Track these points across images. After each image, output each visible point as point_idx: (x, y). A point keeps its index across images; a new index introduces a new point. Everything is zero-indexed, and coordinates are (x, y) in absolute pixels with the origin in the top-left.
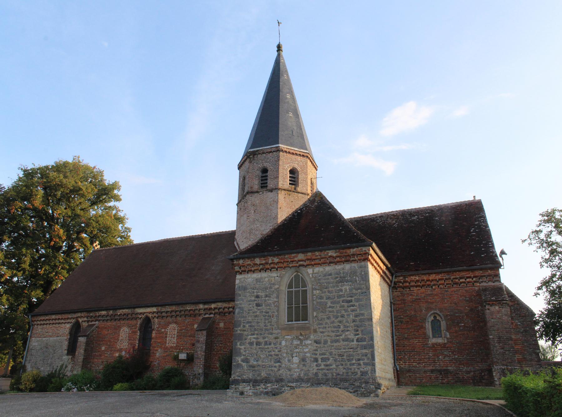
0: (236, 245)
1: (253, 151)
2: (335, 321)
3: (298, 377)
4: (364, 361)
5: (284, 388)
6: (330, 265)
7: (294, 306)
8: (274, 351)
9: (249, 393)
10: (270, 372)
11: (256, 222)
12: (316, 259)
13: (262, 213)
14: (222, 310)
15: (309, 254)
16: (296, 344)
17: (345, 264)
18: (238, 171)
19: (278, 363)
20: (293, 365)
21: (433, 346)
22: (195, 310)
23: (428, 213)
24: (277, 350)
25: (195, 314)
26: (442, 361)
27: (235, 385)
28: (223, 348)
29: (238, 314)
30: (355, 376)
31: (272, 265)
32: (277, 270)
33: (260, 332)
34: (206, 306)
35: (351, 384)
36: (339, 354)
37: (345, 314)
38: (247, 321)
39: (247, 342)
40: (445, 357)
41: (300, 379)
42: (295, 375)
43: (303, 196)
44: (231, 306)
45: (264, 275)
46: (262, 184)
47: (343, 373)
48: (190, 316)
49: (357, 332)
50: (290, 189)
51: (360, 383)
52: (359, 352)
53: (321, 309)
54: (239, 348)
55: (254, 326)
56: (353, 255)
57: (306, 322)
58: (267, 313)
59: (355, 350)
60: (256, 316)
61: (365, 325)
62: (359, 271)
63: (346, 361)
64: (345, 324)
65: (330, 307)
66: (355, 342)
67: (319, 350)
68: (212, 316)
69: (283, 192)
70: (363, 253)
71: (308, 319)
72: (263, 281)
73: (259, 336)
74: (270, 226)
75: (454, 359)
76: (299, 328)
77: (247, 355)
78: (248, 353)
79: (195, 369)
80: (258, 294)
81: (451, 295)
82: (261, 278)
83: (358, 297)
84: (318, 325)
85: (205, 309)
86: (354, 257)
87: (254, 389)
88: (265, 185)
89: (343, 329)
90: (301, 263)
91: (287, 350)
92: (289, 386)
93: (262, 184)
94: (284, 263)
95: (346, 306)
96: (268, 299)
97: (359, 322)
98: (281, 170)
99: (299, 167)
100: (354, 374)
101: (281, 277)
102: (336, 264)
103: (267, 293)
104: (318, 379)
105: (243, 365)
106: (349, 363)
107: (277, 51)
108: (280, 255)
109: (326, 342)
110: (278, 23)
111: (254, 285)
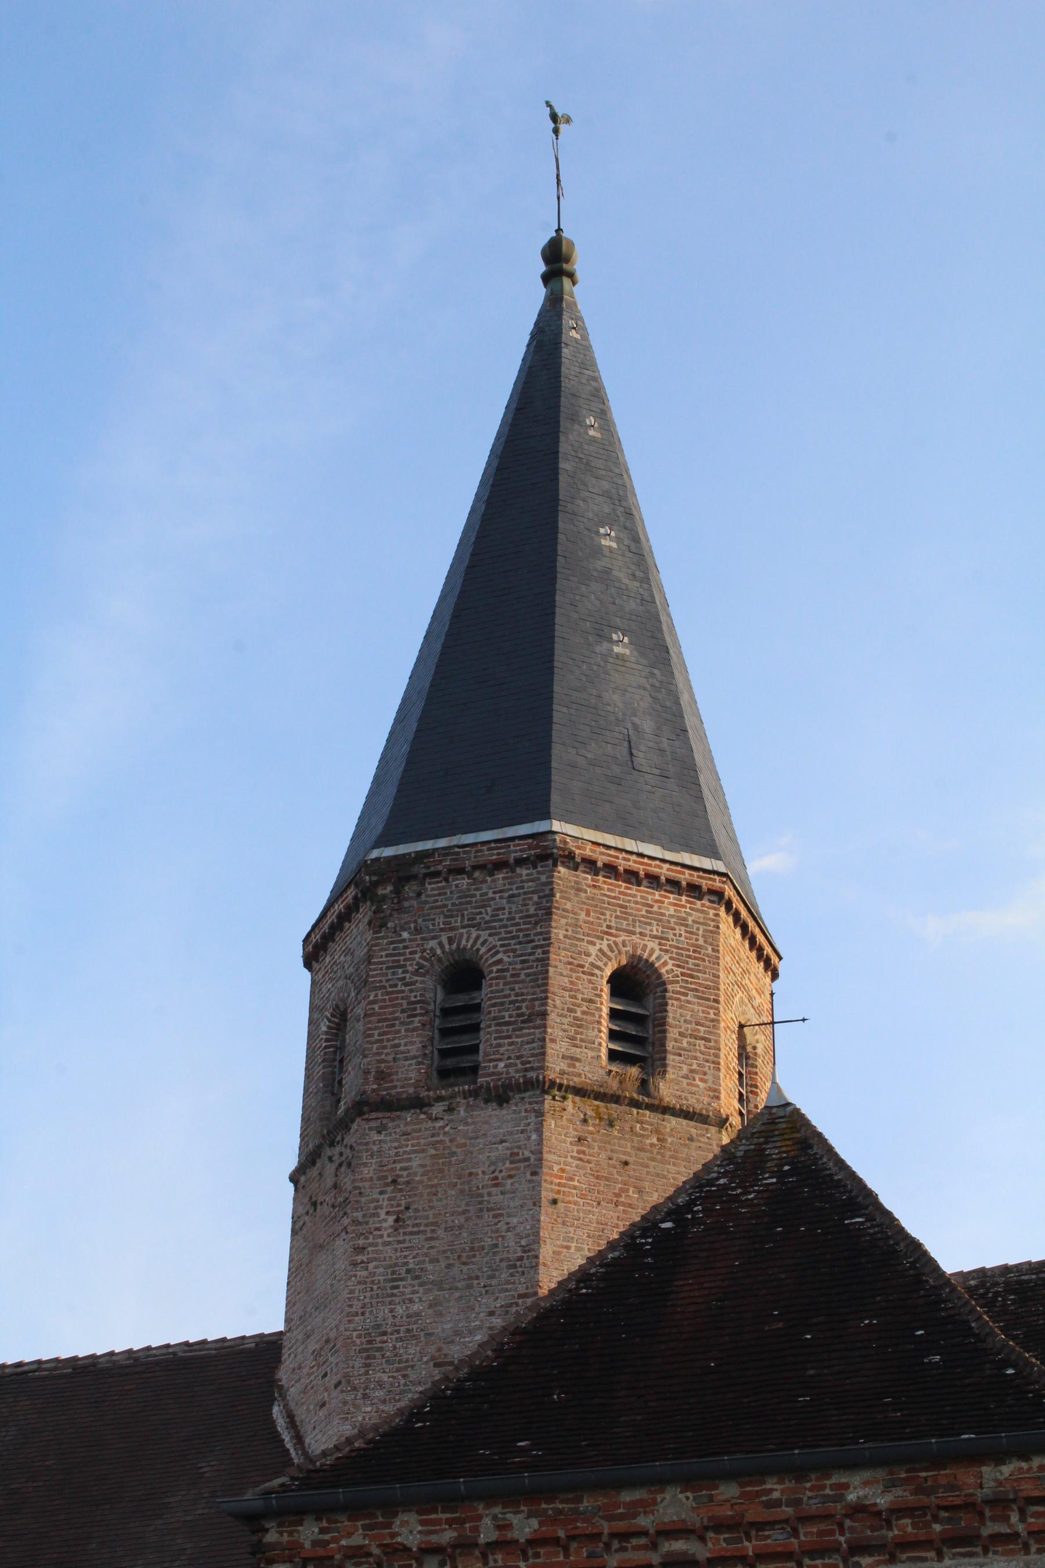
1: (395, 857)
11: (406, 1287)
12: (771, 1524)
15: (728, 1491)
46: (444, 1053)
56: (1000, 1503)
74: (491, 1314)
86: (1006, 1519)
88: (465, 1062)
93: (444, 1053)
94: (574, 1545)
98: (559, 975)
99: (666, 957)
107: (546, 278)
108: (550, 1493)
110: (554, 117)
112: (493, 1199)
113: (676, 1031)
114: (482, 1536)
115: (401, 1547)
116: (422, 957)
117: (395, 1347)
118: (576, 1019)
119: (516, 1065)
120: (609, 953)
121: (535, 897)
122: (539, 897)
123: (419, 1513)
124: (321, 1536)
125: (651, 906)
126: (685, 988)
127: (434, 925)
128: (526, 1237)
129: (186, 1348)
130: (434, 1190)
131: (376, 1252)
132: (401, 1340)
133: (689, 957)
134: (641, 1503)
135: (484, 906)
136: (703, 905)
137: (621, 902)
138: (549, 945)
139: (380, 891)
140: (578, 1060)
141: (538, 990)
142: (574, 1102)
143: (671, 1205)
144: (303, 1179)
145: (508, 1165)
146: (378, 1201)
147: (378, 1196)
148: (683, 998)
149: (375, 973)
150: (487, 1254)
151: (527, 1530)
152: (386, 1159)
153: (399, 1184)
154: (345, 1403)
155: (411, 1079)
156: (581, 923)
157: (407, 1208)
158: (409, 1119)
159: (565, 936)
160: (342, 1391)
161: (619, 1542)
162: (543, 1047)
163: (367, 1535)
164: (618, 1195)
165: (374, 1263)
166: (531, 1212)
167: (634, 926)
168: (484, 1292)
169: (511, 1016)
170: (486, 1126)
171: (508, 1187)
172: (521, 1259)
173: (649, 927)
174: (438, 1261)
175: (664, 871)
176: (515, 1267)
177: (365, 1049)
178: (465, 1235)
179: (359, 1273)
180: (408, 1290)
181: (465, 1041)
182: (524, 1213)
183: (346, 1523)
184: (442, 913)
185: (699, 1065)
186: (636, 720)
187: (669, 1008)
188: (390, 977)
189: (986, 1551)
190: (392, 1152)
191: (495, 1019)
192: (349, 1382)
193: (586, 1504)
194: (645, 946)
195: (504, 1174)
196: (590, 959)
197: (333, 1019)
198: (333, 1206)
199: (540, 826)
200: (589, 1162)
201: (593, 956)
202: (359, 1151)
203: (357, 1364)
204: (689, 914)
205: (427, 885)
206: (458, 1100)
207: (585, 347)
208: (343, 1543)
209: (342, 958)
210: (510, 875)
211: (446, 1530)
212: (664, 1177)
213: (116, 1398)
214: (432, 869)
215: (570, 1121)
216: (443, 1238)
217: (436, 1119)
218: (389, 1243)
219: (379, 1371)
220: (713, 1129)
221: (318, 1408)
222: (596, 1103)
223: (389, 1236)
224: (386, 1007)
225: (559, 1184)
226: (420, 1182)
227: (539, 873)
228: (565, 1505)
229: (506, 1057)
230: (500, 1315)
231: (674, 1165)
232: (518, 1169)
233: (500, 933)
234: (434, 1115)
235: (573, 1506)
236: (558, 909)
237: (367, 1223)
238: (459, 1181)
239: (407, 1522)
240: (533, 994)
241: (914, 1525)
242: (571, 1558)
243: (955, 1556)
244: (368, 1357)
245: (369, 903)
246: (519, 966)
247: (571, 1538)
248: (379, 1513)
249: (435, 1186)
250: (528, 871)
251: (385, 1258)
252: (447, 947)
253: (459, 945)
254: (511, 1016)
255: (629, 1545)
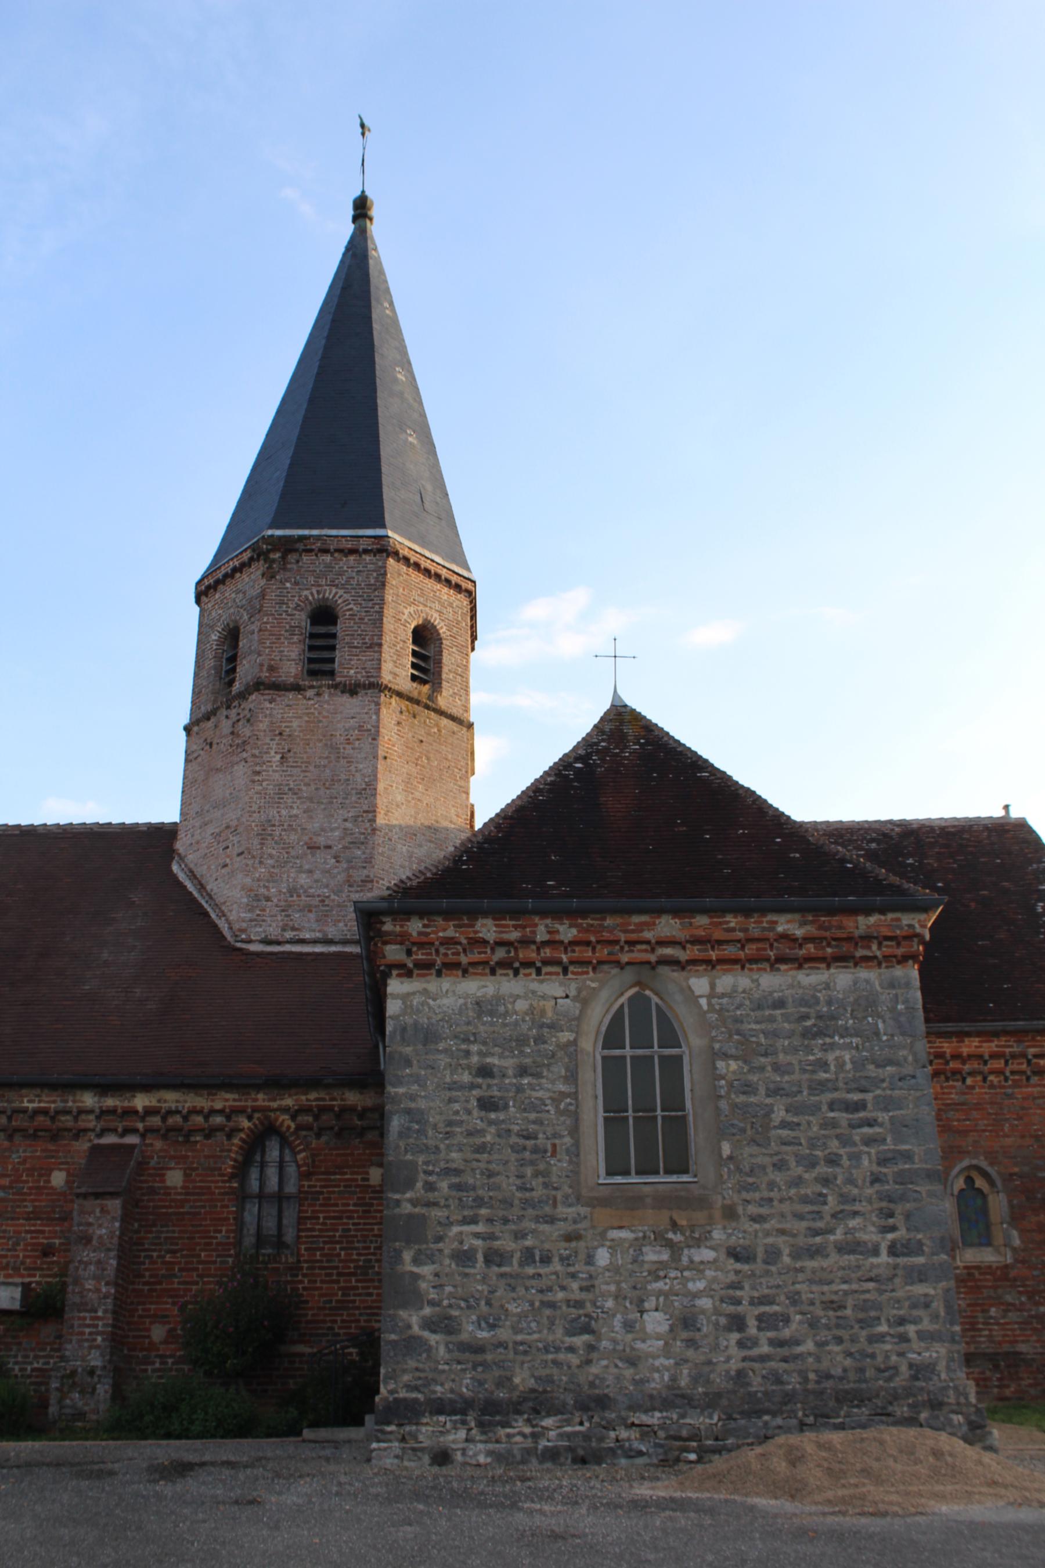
0: (182, 877)
1: (284, 537)
2: (806, 1176)
3: (669, 1388)
4: (920, 1327)
5: (612, 1434)
6: (778, 970)
7: (630, 1113)
8: (563, 1288)
9: (475, 1455)
10: (548, 1371)
11: (289, 799)
12: (727, 942)
13: (311, 768)
14: (178, 1119)
15: (702, 920)
16: (656, 1262)
17: (832, 971)
18: (197, 609)
19: (580, 1334)
20: (644, 1341)
21: (969, 1274)
22: (58, 1112)
23: (872, 840)
24: (575, 1286)
25: (59, 1130)
26: (998, 1324)
27: (400, 1425)
28: (181, 1270)
29: (401, 1134)
30: (889, 1379)
31: (547, 952)
32: (565, 971)
33: (501, 1213)
34: (110, 1102)
35: (879, 1411)
36: (825, 1298)
37: (842, 1151)
38: (443, 1165)
39: (447, 1252)
40: (1006, 1311)
41: (676, 1396)
42: (657, 1383)
43: (455, 729)
44: (218, 1105)
45: (508, 985)
46: (311, 661)
47: (845, 1370)
48: (35, 1136)
49: (891, 1221)
50: (415, 695)
51: (912, 1406)
52: (900, 1294)
53: (749, 1132)
54: (412, 1273)
55: (474, 1188)
56: (867, 939)
57: (685, 1178)
58: (527, 1137)
59: (884, 1287)
60: (481, 1149)
61: (915, 1195)
62: (885, 996)
63: (852, 1327)
64: (845, 1190)
65: (784, 1125)
66: (884, 1258)
67: (747, 1287)
68: (132, 1140)
70: (904, 934)
71: (692, 1167)
73: (497, 1228)
74: (345, 820)
75: (1036, 1317)
76: (663, 1201)
77: (445, 1303)
78: (451, 1296)
79: (69, 1349)
80: (488, 1060)
81: (1023, 1108)
82: (498, 998)
83: (889, 1092)
84: (739, 1192)
85: (104, 1113)
86: (869, 948)
87: (483, 1438)
88: (326, 667)
89: (838, 1209)
90: (668, 951)
91: (618, 1283)
92: (633, 1424)
93: (311, 661)
94: (599, 947)
95: (844, 1123)
96: (529, 1084)
97: (896, 1183)
98: (388, 623)
99: (442, 624)
100: (886, 1374)
101: (584, 1000)
102: (800, 967)
103: (528, 1061)
104: (752, 1395)
105: (433, 1343)
106: (864, 1333)
107: (355, 219)
108: (583, 913)
109: (773, 1255)
110: (363, 126)
111: (468, 1023)
112: (346, 752)
123: (494, 919)
132: (285, 830)
144: (196, 729)
154: (247, 865)
157: (289, 751)
162: (380, 664)
164: (417, 759)
172: (365, 789)
178: (328, 771)
180: (290, 801)
181: (326, 655)
189: (856, 965)
190: (280, 716)
199: (380, 532)
207: (379, 262)
208: (441, 934)
209: (233, 595)
220: (465, 729)
226: (298, 736)
241: (815, 948)
243: (837, 967)
245: (262, 562)
247: (598, 942)
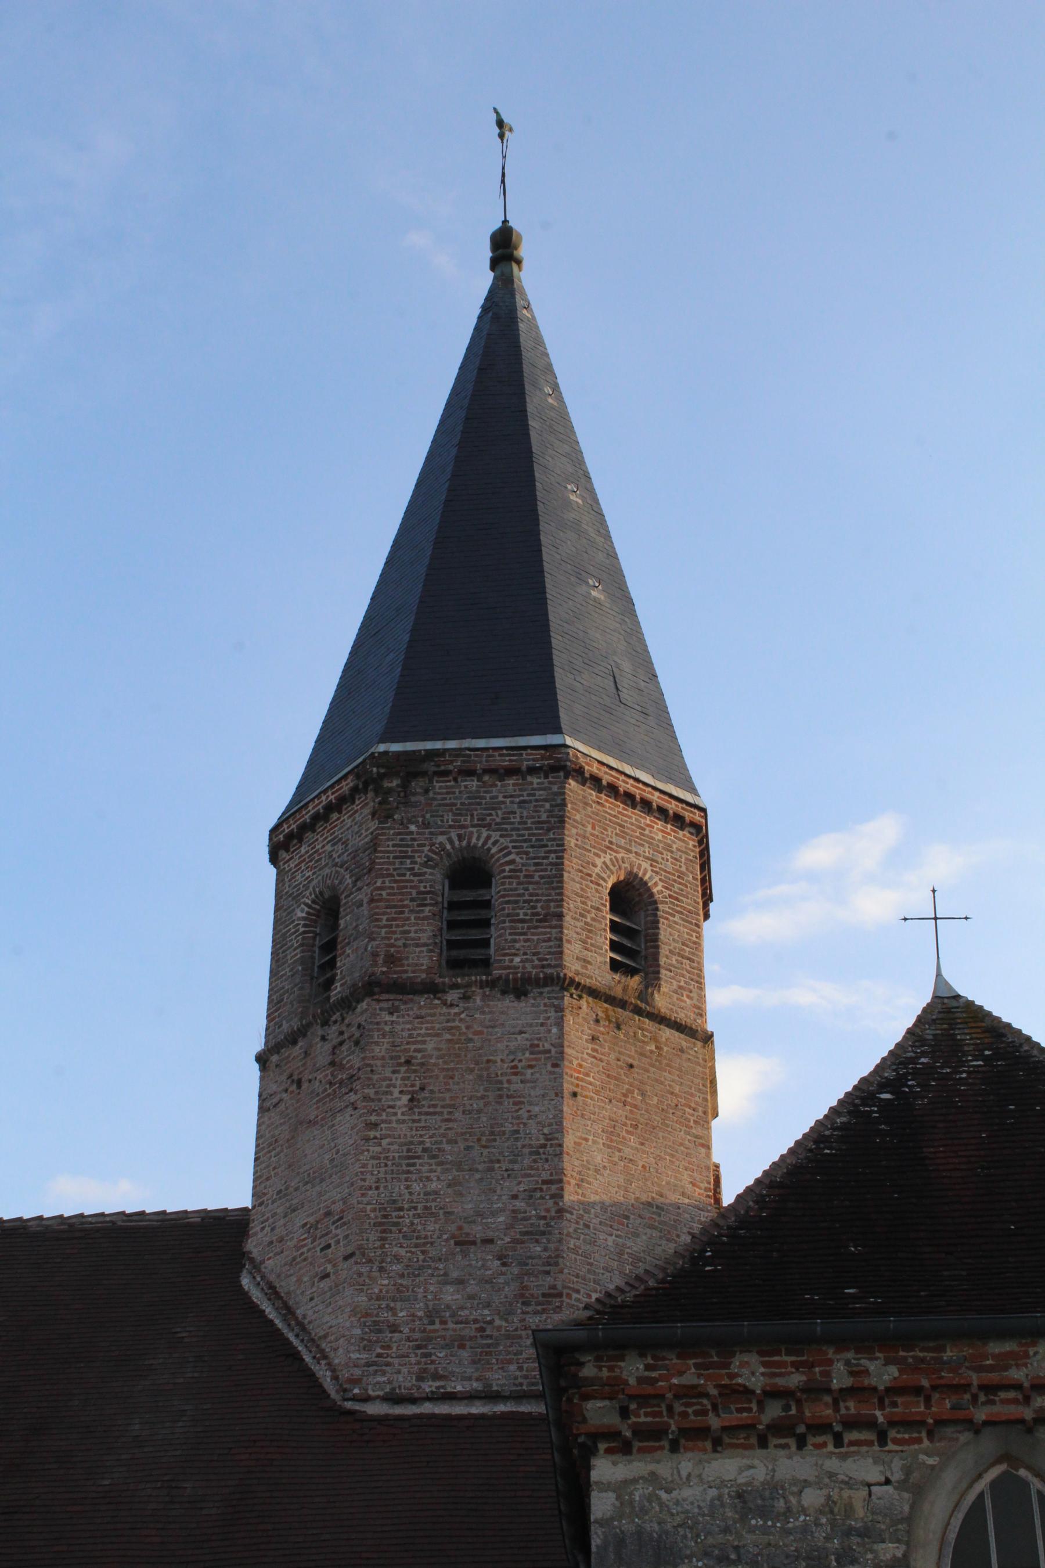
0: (256, 1295)
1: (405, 753)
13: (458, 1115)
31: (851, 1407)
69: (586, 1003)
72: (789, 1509)
74: (515, 1197)
82: (774, 1488)
88: (476, 954)
93: (452, 944)
94: (936, 1396)
98: (572, 882)
99: (656, 879)
107: (494, 264)
110: (500, 123)
112: (513, 1087)
113: (667, 948)
114: (835, 1381)
115: (741, 1389)
116: (430, 850)
117: (412, 1224)
118: (586, 923)
119: (533, 961)
120: (612, 867)
121: (547, 805)
122: (551, 806)
123: (761, 1353)
124: (647, 1373)
125: (644, 830)
126: (672, 909)
127: (442, 821)
128: (549, 1126)
129: (125, 1218)
130: (450, 1073)
131: (389, 1129)
132: (419, 1216)
133: (675, 881)
134: (1011, 1354)
135: (494, 809)
136: (684, 835)
137: (619, 821)
138: (563, 851)
139: (386, 784)
140: (589, 963)
141: (553, 892)
142: (588, 1003)
143: (879, 1079)
144: (275, 1058)
145: (527, 1055)
146: (391, 1080)
147: (391, 1075)
148: (671, 918)
149: (381, 860)
150: (508, 1139)
151: (886, 1377)
152: (399, 1040)
153: (413, 1065)
154: (360, 1275)
155: (422, 965)
156: (588, 835)
157: (422, 1089)
158: (422, 1003)
159: (576, 845)
160: (356, 1263)
161: (986, 1395)
162: (560, 946)
163: (702, 1375)
165: (387, 1140)
166: (554, 1102)
167: (631, 845)
168: (506, 1176)
169: (526, 914)
170: (503, 1017)
171: (528, 1076)
172: (544, 1146)
173: (642, 849)
174: (456, 1142)
175: (655, 798)
176: (538, 1153)
177: (373, 933)
179: (371, 1148)
180: (426, 1168)
181: (475, 934)
182: (546, 1102)
183: (675, 1361)
184: (451, 810)
185: (686, 983)
186: (616, 659)
187: (660, 925)
188: (397, 866)
190: (405, 1034)
191: (508, 915)
192: (363, 1255)
193: (949, 1353)
194: (640, 865)
195: (523, 1064)
196: (597, 870)
197: (314, 906)
198: (331, 1084)
200: (601, 1060)
201: (599, 868)
202: (369, 1030)
203: (372, 1238)
204: (674, 842)
205: (435, 784)
206: (474, 989)
208: (675, 1381)
210: (520, 781)
211: (793, 1373)
212: (662, 1083)
213: (59, 1260)
214: (443, 768)
215: (584, 1019)
216: (461, 1121)
217: (452, 1005)
218: (404, 1122)
219: (396, 1245)
220: (699, 1044)
221: (316, 1280)
222: (606, 1005)
223: (403, 1114)
224: (394, 894)
225: (577, 1078)
227: (550, 783)
228: (926, 1354)
229: (522, 952)
230: (523, 1199)
231: (670, 1073)
232: (536, 1060)
233: (512, 835)
234: (449, 1002)
235: (935, 1355)
236: (570, 818)
237: (380, 1100)
238: (477, 1067)
239: (747, 1363)
240: (547, 896)
242: (933, 1409)
244: (384, 1231)
245: (371, 795)
246: (533, 868)
247: (934, 1388)
248: (713, 1352)
249: (453, 1069)
250: (539, 780)
251: (400, 1135)
252: (457, 843)
253: (469, 843)
254: (526, 914)
255: (997, 1399)
